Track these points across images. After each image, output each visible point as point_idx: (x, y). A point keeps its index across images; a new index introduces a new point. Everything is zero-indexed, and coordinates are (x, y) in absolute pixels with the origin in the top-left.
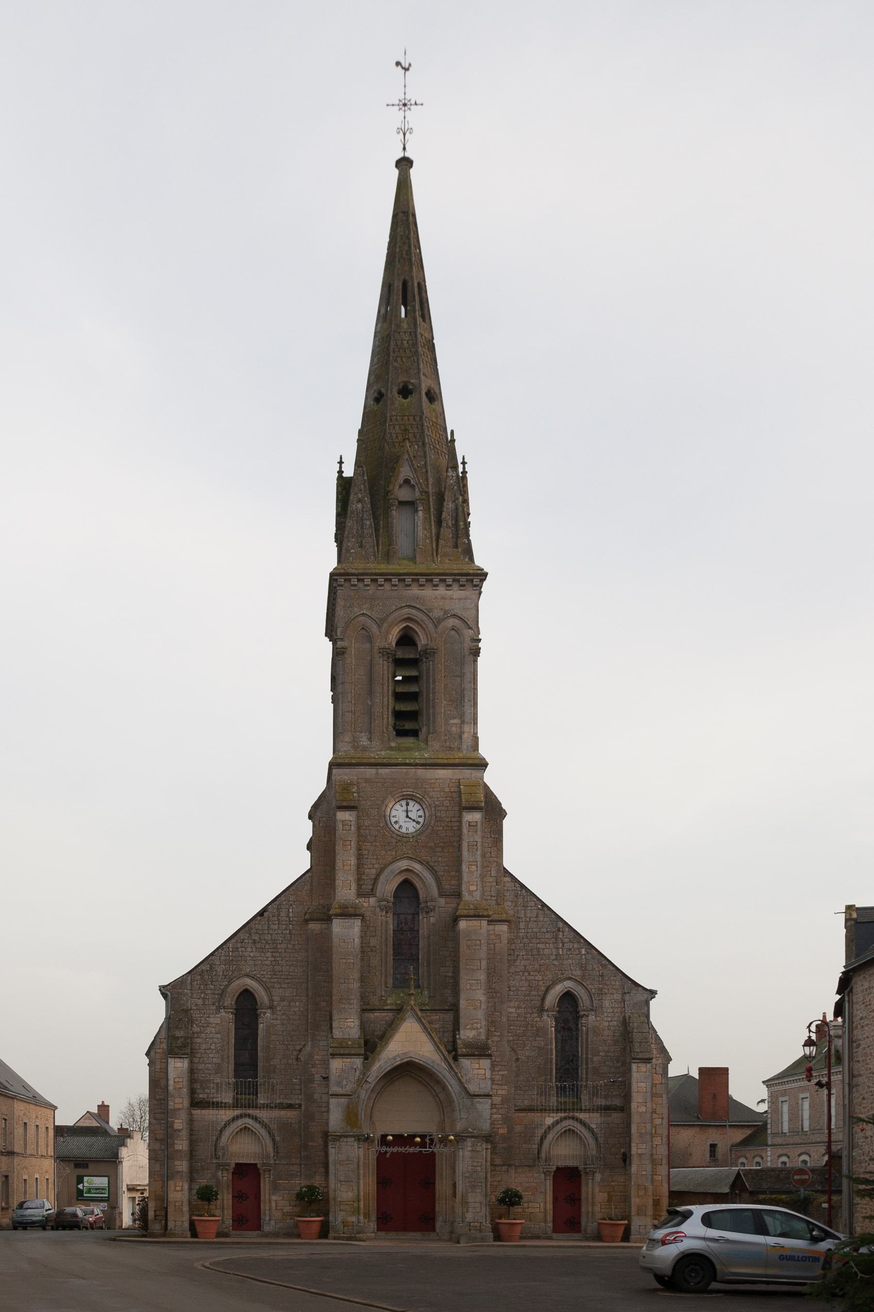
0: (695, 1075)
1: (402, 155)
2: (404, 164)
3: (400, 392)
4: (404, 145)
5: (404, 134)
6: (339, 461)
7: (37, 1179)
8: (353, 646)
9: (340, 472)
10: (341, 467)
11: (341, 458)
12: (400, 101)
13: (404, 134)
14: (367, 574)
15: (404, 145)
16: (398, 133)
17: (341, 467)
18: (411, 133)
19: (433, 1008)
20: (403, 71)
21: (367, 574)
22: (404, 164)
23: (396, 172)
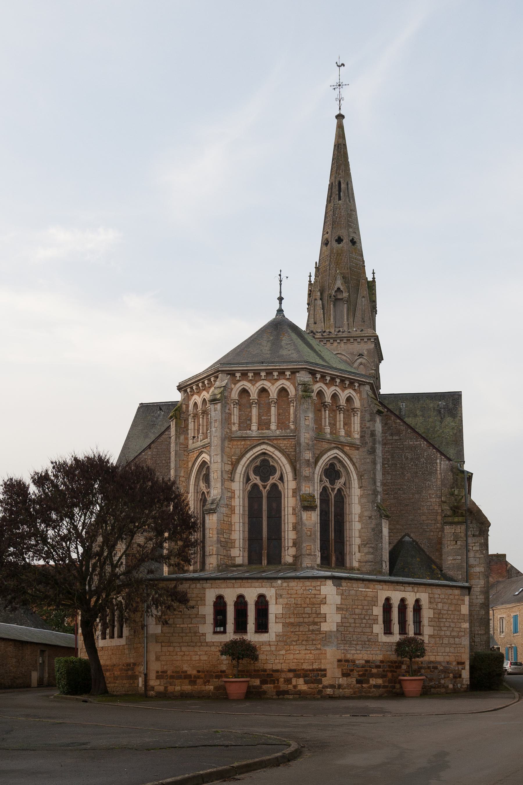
0: (69, 462)
1: (339, 113)
2: (340, 117)
3: (336, 241)
4: (340, 107)
5: (340, 101)
6: (279, 296)
7: (340, 199)
8: (386, 625)
9: (310, 281)
10: (374, 276)
11: (310, 274)
12: (337, 83)
13: (340, 101)
14: (351, 337)
15: (340, 107)
16: (337, 101)
17: (374, 276)
18: (343, 100)
19: (323, 321)
20: (338, 68)
21: (351, 337)
22: (340, 117)
23: (336, 121)
